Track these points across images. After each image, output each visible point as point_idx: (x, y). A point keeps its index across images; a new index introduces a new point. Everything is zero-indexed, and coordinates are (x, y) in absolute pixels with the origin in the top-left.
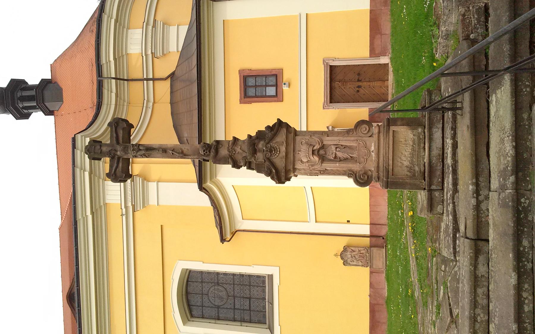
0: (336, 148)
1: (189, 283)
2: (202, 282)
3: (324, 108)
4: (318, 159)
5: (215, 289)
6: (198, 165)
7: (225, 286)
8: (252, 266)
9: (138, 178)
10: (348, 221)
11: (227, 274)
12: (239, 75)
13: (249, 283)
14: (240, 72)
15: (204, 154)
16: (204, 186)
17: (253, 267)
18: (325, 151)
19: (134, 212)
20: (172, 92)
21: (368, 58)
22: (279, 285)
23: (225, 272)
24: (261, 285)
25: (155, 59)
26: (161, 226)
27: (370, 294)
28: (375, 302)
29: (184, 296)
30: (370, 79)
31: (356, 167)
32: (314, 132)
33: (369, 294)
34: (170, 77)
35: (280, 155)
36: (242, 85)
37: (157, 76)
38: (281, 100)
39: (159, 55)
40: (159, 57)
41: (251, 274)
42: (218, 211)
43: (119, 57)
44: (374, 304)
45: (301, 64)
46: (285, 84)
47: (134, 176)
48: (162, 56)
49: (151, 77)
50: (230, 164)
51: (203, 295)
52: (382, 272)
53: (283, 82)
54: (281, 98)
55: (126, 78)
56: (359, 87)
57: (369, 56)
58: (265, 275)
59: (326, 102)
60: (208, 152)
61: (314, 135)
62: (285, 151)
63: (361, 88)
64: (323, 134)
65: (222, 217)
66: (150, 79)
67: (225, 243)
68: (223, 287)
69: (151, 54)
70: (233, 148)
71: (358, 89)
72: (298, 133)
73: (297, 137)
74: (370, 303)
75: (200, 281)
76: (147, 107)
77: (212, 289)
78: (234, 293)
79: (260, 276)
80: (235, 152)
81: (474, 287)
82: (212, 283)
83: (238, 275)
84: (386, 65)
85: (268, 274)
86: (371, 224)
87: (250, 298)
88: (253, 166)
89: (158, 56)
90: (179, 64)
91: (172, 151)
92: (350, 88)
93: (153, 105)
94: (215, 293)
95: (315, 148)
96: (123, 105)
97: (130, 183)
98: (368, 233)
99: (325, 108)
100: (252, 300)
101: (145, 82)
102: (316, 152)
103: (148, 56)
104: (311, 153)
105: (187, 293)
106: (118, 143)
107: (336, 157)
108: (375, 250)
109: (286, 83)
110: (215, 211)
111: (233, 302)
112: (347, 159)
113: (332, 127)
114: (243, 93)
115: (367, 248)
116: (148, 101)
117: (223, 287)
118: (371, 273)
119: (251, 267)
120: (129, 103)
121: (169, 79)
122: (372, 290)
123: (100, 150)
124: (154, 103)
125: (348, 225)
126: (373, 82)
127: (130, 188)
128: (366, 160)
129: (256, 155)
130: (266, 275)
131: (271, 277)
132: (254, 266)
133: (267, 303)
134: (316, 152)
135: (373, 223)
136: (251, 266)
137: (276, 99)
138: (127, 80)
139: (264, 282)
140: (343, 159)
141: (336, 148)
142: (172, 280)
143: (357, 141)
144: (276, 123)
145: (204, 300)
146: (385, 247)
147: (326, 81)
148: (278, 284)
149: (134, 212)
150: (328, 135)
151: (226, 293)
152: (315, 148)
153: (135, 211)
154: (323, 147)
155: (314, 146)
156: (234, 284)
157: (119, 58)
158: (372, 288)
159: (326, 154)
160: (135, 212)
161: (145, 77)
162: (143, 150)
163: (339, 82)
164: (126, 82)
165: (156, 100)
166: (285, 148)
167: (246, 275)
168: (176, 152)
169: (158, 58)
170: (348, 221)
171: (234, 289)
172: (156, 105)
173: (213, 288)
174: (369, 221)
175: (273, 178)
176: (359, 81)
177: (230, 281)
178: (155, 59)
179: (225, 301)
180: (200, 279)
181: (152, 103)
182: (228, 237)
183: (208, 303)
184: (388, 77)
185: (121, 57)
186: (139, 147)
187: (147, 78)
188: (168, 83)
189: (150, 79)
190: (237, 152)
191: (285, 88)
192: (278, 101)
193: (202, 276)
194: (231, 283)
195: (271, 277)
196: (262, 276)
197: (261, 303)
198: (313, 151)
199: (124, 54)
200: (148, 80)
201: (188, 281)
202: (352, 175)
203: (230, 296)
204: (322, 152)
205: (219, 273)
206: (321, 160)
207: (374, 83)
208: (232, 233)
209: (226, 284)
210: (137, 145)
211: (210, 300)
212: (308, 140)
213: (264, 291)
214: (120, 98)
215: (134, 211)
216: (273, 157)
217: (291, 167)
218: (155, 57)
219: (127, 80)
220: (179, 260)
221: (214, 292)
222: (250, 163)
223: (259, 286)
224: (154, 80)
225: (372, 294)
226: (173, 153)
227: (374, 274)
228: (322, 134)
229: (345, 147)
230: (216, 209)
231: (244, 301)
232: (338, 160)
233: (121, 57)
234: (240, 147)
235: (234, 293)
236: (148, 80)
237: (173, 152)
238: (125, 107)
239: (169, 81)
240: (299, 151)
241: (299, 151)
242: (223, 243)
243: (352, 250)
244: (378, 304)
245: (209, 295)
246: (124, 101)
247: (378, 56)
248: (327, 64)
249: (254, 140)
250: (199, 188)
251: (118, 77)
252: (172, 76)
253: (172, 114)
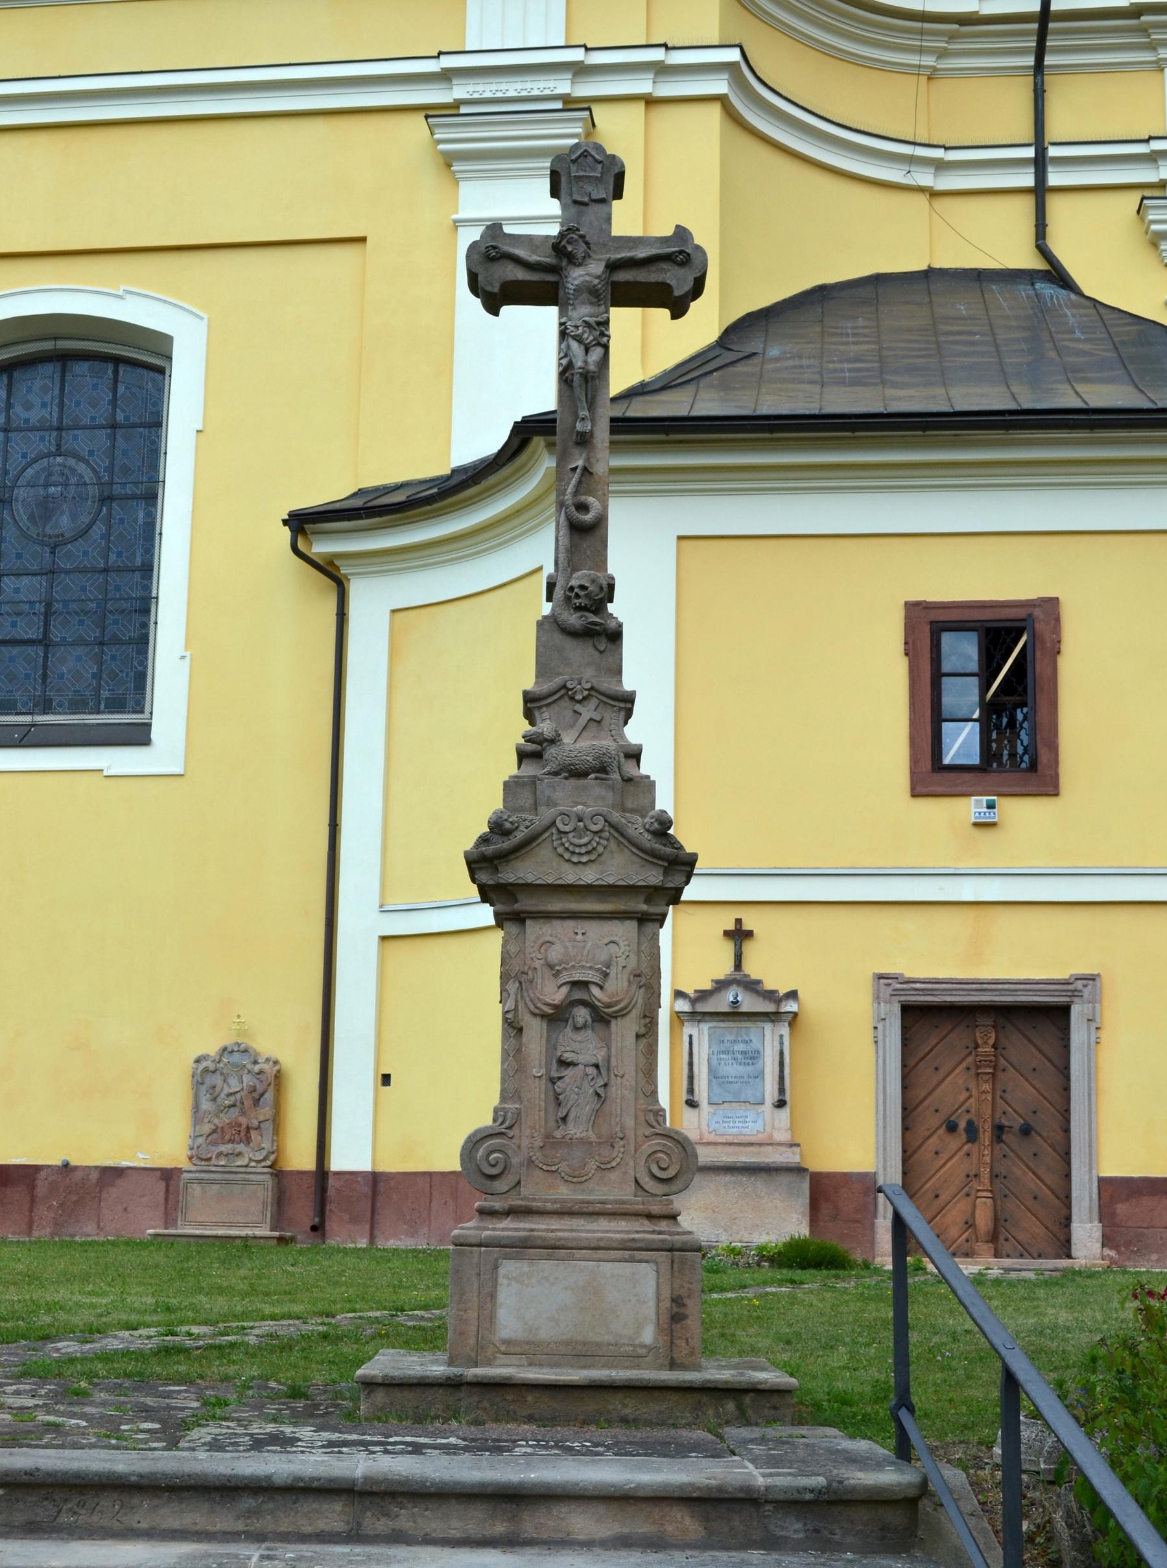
0: (597, 1066)
1: (110, 368)
2: (114, 426)
3: (881, 977)
4: (556, 1002)
5: (85, 484)
6: (630, 414)
7: (99, 529)
8: (188, 654)
9: (580, 130)
10: (386, 1079)
11: (152, 539)
12: (1034, 597)
13: (109, 640)
14: (1051, 605)
15: (572, 589)
16: (538, 442)
17: (183, 657)
18: (585, 1026)
19: (423, 114)
20: (979, 276)
21: (1094, 1172)
22: (105, 773)
23: (158, 531)
24: (105, 694)
25: (1134, 198)
26: (362, 240)
27: (76, 1168)
28: (41, 1189)
29: (48, 345)
30: (1005, 1177)
31: (527, 1139)
32: (656, 987)
33: (74, 1162)
34: (1050, 268)
35: (567, 867)
36: (988, 611)
37: (1057, 206)
38: (919, 789)
39: (1151, 217)
40: (1142, 220)
41: (156, 570)
42: (429, 500)
43: (1146, 31)
44: (32, 1187)
45: (1067, 877)
46: (991, 806)
47: (589, 109)
48: (1147, 233)
49: (1054, 178)
50: (536, 683)
51: (55, 434)
52: (169, 1221)
53: (997, 795)
54: (939, 789)
55: (1049, 60)
56: (972, 1133)
57: (1102, 1175)
58: (147, 709)
59: (905, 986)
60: (580, 600)
61: (640, 987)
62: (582, 883)
63: (968, 1141)
64: (648, 1020)
65: (400, 519)
66: (1041, 176)
67: (286, 532)
68: (93, 522)
69: (1157, 180)
70: (593, 693)
71: (962, 1125)
72: (650, 927)
73: (634, 924)
74: (37, 1169)
75: (120, 417)
76: (911, 160)
77: (82, 468)
78: (68, 572)
79: (144, 688)
80: (579, 702)
81: (40, 366)
82: (110, 469)
83: (148, 588)
84: (1065, 1248)
85: (149, 725)
86: (375, 1178)
87: (45, 642)
88: (530, 769)
89: (1151, 212)
90: (1100, 308)
91: (585, 469)
92: (965, 1095)
93: (921, 189)
94: (66, 485)
95: (595, 991)
96: (921, 51)
97: (557, 92)
98: (338, 1162)
99: (882, 981)
100: (40, 651)
101: (1030, 153)
102: (579, 995)
103: (1153, 166)
104: (576, 979)
105: (64, 358)
106: (613, 266)
107: (564, 1064)
108: (264, 1189)
109: (995, 810)
110: (431, 484)
111: (28, 569)
112: (559, 1105)
113: (795, 1014)
114: (955, 615)
115: (272, 1157)
116: (940, 166)
117: (93, 522)
118: (168, 1176)
119: (183, 648)
120: (933, 75)
121: (1036, 263)
122: (95, 1176)
123: (586, 199)
124: (934, 194)
125: (369, 1079)
126: (991, 1191)
127: (536, 92)
128: (553, 1168)
129: (566, 778)
130: (147, 715)
131: (139, 736)
132: (188, 659)
133: (27, 719)
134: (579, 995)
135: (381, 1187)
136: (186, 649)
137: (927, 764)
138: (1039, 67)
139: (117, 705)
140: (559, 1090)
141: (597, 1066)
142: (121, 293)
143: (621, 1139)
144: (681, 848)
145: (34, 436)
146: (277, 1234)
147: (1000, 986)
148: (109, 768)
149: (423, 114)
150: (643, 1035)
151: (67, 535)
152: (595, 991)
153: (429, 120)
154: (602, 1018)
155: (601, 988)
156: (106, 570)
157: (1144, 30)
158: (100, 1180)
159: (577, 1029)
160: (427, 117)
161: (1053, 152)
162: (586, 362)
163: (994, 1046)
164: (1030, 61)
165: (942, 204)
166: (589, 882)
167: (145, 625)
168: (580, 482)
169: (1138, 212)
170: (386, 1079)
171: (84, 571)
172: (922, 200)
173: (88, 476)
174: (387, 1170)
175: (483, 840)
176: (999, 1130)
177: (119, 555)
178: (1134, 198)
179: (33, 532)
180: (127, 418)
181: (930, 184)
182: (321, 548)
183: (24, 456)
184: (1008, 1256)
185: (1149, 36)
186: (599, 344)
187: (1048, 160)
188: (1026, 259)
189: (1041, 176)
190: (578, 707)
191: (972, 807)
192: (913, 773)
193: (141, 425)
194: (112, 557)
195: (139, 736)
196: (144, 698)
197: (26, 690)
198: (584, 985)
199: (1160, 51)
200: (1040, 163)
201: (117, 360)
202: (500, 1120)
203: (53, 553)
204: (582, 1015)
205: (155, 505)
206: (550, 1011)
207: (989, 1195)
208: (331, 563)
209: (107, 536)
210: (605, 339)
211: (35, 461)
212: (624, 967)
213: (78, 706)
214: (952, 37)
215: (429, 112)
216: (559, 842)
217: (525, 903)
218: (1143, 198)
219: (1039, 67)
220: (209, 319)
221: (73, 480)
222: (537, 756)
223: (99, 687)
224: (1040, 192)
225: (78, 1176)
226: (574, 469)
227: (162, 1185)
228: (645, 1016)
229: (599, 1095)
230: (435, 490)
231: (34, 614)
232: (555, 1074)
233: (1149, 36)
234: (598, 719)
235: (68, 572)
236: (1040, 163)
237: (578, 471)
238: (913, 59)
239: (1036, 263)
240: (583, 934)
241: (583, 934)
242: (285, 522)
243: (262, 1095)
244: (33, 1201)
245: (59, 459)
246: (942, 54)
247: (1106, 1214)
248: (1076, 993)
249: (619, 768)
250: (526, 421)
251: (1051, 25)
252: (1057, 276)
253: (878, 280)
